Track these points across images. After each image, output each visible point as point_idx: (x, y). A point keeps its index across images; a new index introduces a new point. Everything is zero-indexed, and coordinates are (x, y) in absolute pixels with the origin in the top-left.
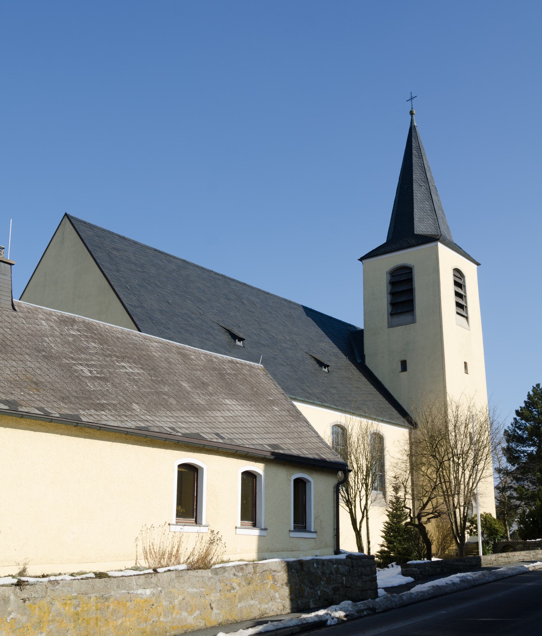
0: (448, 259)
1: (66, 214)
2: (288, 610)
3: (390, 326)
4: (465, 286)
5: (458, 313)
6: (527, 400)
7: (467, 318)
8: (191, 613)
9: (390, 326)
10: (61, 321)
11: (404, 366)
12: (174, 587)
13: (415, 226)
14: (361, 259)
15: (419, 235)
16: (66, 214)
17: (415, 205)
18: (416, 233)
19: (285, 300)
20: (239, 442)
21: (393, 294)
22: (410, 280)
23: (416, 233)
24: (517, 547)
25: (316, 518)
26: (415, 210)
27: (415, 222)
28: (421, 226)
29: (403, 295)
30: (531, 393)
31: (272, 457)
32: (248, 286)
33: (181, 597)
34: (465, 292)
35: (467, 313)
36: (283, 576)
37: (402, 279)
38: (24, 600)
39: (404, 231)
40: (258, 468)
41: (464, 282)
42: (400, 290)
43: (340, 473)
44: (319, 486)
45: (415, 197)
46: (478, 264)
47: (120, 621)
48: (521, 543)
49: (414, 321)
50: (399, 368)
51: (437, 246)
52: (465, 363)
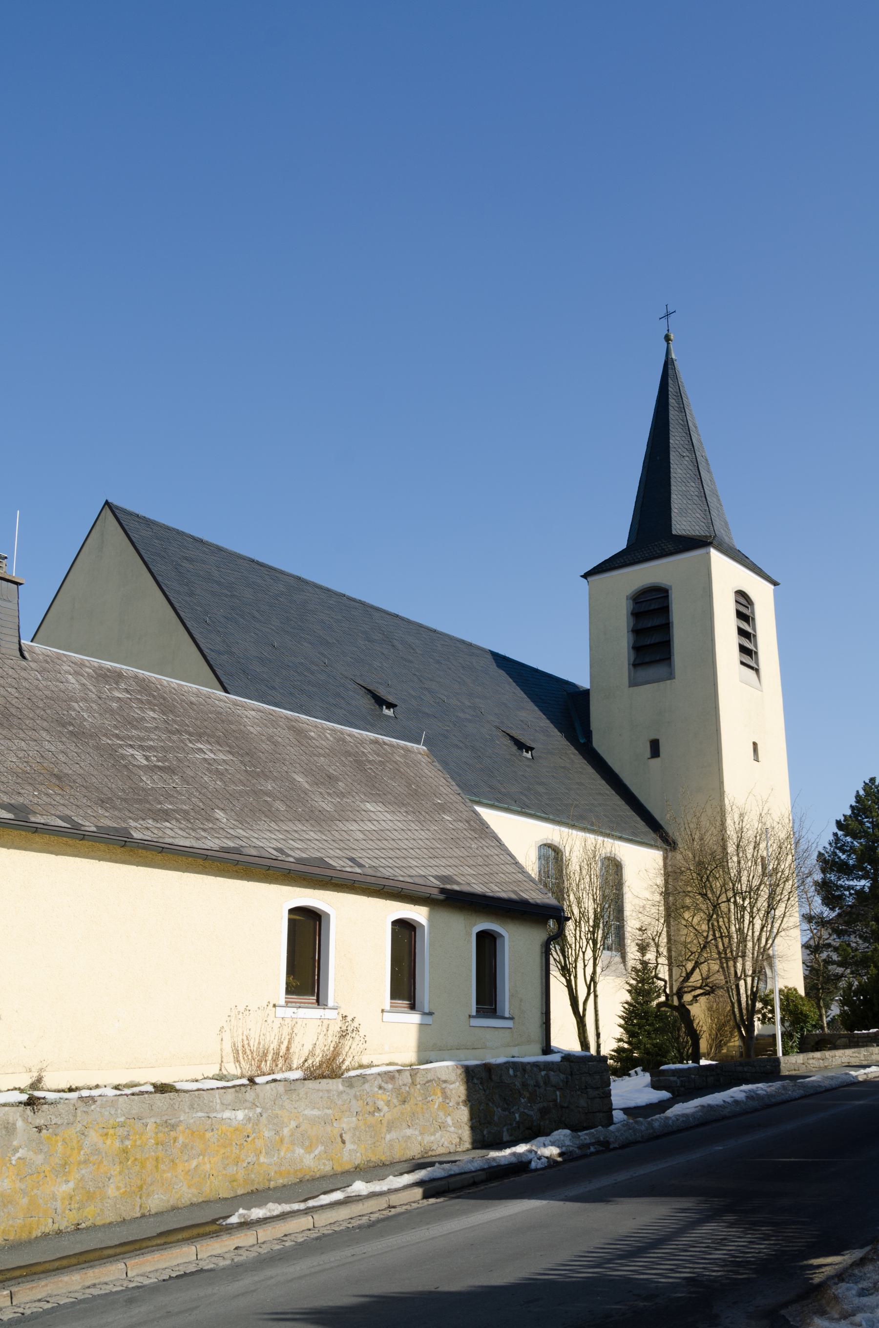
0: (726, 575)
1: (107, 503)
2: (468, 1145)
3: (633, 683)
4: (753, 619)
5: (742, 663)
6: (854, 804)
7: (757, 671)
8: (309, 1149)
9: (633, 683)
10: (99, 675)
11: (655, 748)
12: (282, 1107)
13: (673, 522)
14: (586, 576)
15: (680, 536)
16: (107, 503)
17: (673, 488)
18: (674, 532)
19: (463, 642)
20: (387, 872)
21: (637, 632)
22: (664, 610)
23: (674, 532)
24: (839, 1042)
25: (512, 996)
26: (673, 496)
27: (673, 515)
28: (683, 523)
29: (653, 634)
30: (862, 793)
31: (442, 897)
32: (402, 619)
33: (293, 1124)
34: (754, 629)
35: (757, 663)
36: (458, 1089)
37: (652, 607)
38: (39, 1129)
39: (655, 530)
40: (418, 914)
41: (753, 612)
42: (649, 625)
43: (551, 922)
44: (518, 943)
45: (673, 475)
46: (775, 584)
47: (194, 1163)
48: (844, 1036)
49: (671, 676)
50: (648, 753)
51: (708, 553)
52: (755, 744)
